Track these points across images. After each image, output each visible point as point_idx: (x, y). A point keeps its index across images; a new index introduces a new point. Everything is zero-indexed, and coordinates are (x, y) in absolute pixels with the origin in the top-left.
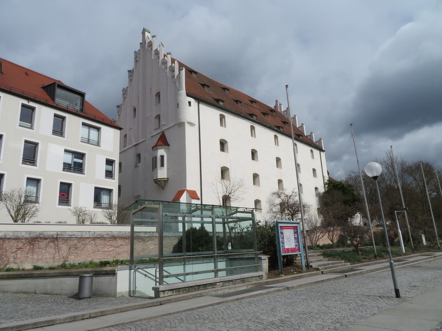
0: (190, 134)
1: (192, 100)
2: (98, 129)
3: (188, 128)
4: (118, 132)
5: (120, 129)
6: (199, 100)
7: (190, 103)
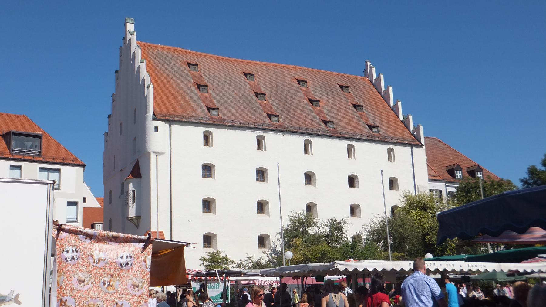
1: (161, 124)
4: (82, 168)
5: (84, 166)
6: (170, 122)
7: (156, 128)
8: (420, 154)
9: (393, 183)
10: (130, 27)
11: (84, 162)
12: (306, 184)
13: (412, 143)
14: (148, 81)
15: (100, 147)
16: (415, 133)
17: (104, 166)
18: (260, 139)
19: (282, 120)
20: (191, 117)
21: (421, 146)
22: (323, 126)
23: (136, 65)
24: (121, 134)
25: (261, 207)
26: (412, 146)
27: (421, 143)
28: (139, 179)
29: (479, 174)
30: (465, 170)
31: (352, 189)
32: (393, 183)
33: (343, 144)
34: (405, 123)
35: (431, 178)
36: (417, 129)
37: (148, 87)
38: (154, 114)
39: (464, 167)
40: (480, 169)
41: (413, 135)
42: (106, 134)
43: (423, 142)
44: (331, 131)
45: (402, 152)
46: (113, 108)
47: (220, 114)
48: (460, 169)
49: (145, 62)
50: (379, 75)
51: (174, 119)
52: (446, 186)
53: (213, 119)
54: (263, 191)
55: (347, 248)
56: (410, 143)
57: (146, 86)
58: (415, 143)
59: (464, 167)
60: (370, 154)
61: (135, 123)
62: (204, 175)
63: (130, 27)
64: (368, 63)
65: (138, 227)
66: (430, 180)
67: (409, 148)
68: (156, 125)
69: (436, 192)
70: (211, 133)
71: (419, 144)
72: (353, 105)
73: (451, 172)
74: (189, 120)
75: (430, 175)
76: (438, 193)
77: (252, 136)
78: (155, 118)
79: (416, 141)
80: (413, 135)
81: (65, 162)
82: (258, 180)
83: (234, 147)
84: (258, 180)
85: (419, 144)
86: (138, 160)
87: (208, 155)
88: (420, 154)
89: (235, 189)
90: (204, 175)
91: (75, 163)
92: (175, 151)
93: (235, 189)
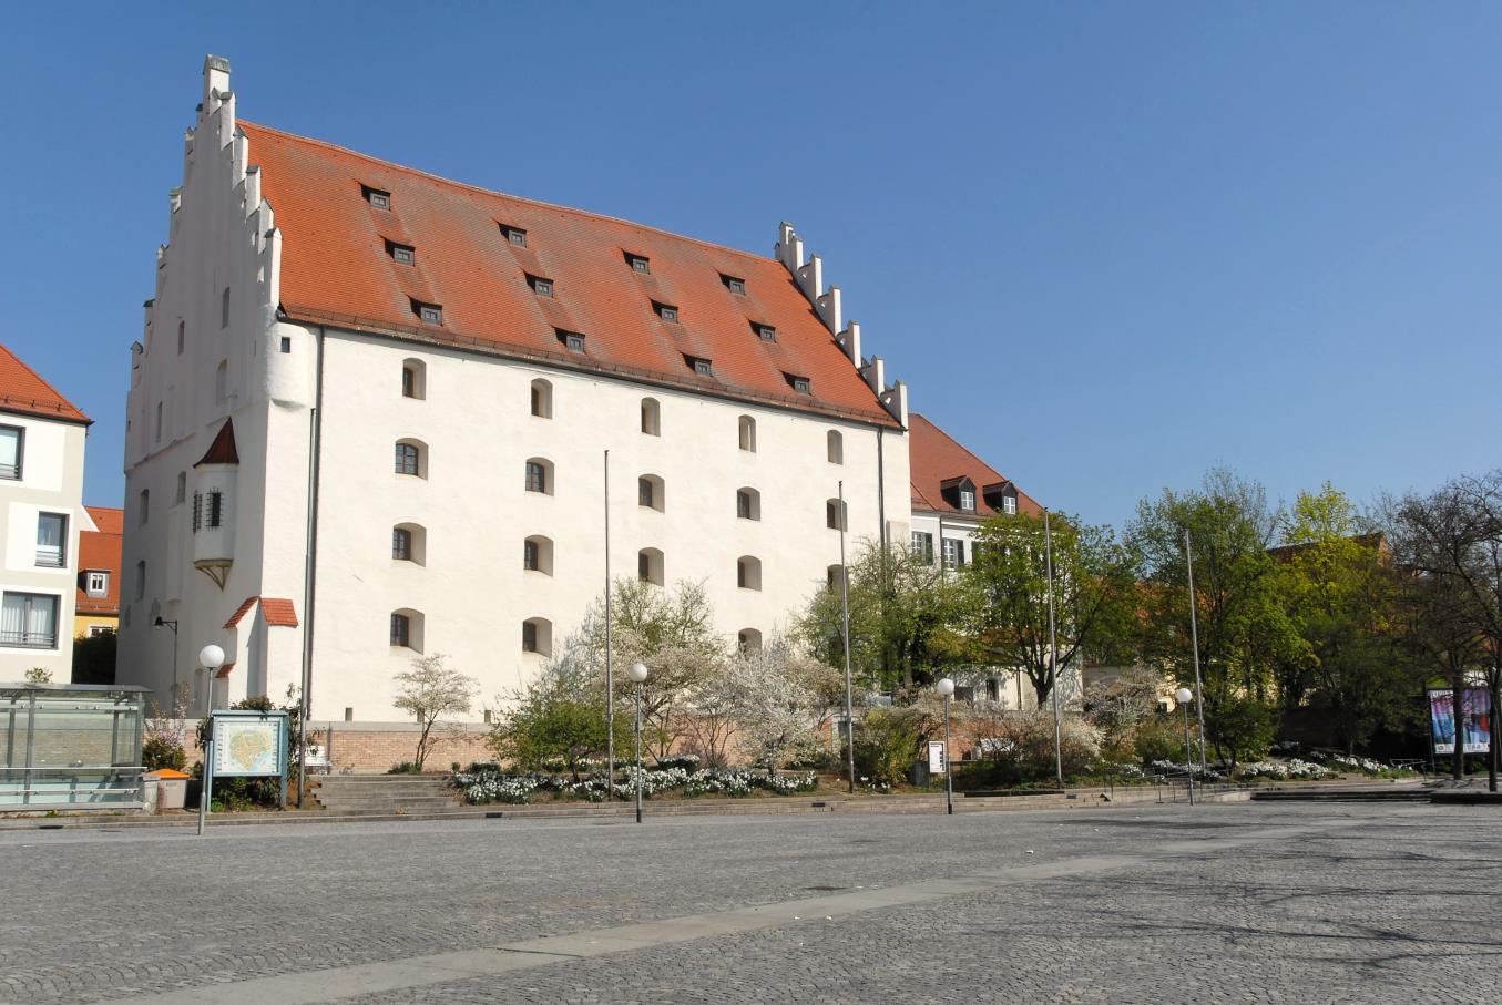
0: (284, 438)
1: (302, 338)
2: (20, 431)
3: (275, 416)
4: (81, 430)
5: (87, 423)
6: (322, 330)
7: (286, 342)
8: (898, 448)
9: (835, 514)
10: (220, 81)
11: (88, 415)
12: (640, 504)
13: (882, 423)
14: (268, 220)
15: (119, 381)
16: (888, 401)
17: (129, 429)
18: (540, 387)
19: (595, 348)
20: (374, 322)
21: (901, 430)
22: (411, 316)
23: (234, 178)
24: (181, 350)
25: (536, 553)
26: (881, 429)
27: (900, 423)
28: (232, 467)
29: (1009, 504)
30: (980, 492)
31: (745, 521)
32: (835, 514)
33: (730, 414)
34: (866, 376)
35: (917, 506)
36: (893, 391)
37: (269, 235)
38: (281, 307)
39: (979, 483)
40: (1013, 492)
41: (881, 404)
42: (139, 349)
43: (905, 423)
44: (575, 358)
45: (858, 441)
46: (162, 283)
47: (446, 321)
48: (970, 487)
49: (259, 173)
50: (813, 258)
51: (333, 324)
52: (941, 526)
53: (424, 328)
54: (537, 515)
55: (1327, 696)
56: (877, 422)
57: (262, 233)
58: (884, 419)
59: (979, 483)
60: (791, 439)
61: (225, 323)
62: (402, 468)
63: (220, 81)
64: (788, 229)
65: (222, 588)
66: (915, 511)
67: (872, 435)
68: (286, 335)
69: (951, 544)
70: (422, 365)
71: (898, 426)
72: (751, 323)
73: (951, 494)
74: (393, 333)
75: (913, 501)
76: (956, 546)
77: (520, 379)
78: (284, 315)
79: (891, 418)
80: (881, 404)
81: (38, 410)
82: (530, 487)
83: (475, 400)
84: (530, 487)
85: (898, 426)
86: (230, 419)
87: (413, 419)
88: (898, 448)
89: (475, 507)
90: (402, 468)
91: (64, 414)
92: (331, 400)
93: (475, 507)
